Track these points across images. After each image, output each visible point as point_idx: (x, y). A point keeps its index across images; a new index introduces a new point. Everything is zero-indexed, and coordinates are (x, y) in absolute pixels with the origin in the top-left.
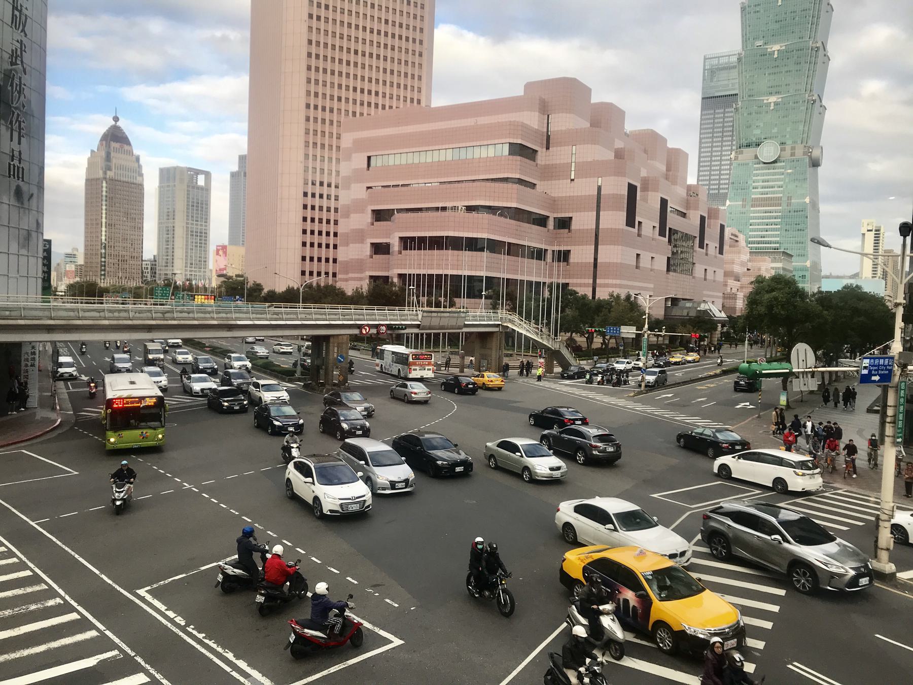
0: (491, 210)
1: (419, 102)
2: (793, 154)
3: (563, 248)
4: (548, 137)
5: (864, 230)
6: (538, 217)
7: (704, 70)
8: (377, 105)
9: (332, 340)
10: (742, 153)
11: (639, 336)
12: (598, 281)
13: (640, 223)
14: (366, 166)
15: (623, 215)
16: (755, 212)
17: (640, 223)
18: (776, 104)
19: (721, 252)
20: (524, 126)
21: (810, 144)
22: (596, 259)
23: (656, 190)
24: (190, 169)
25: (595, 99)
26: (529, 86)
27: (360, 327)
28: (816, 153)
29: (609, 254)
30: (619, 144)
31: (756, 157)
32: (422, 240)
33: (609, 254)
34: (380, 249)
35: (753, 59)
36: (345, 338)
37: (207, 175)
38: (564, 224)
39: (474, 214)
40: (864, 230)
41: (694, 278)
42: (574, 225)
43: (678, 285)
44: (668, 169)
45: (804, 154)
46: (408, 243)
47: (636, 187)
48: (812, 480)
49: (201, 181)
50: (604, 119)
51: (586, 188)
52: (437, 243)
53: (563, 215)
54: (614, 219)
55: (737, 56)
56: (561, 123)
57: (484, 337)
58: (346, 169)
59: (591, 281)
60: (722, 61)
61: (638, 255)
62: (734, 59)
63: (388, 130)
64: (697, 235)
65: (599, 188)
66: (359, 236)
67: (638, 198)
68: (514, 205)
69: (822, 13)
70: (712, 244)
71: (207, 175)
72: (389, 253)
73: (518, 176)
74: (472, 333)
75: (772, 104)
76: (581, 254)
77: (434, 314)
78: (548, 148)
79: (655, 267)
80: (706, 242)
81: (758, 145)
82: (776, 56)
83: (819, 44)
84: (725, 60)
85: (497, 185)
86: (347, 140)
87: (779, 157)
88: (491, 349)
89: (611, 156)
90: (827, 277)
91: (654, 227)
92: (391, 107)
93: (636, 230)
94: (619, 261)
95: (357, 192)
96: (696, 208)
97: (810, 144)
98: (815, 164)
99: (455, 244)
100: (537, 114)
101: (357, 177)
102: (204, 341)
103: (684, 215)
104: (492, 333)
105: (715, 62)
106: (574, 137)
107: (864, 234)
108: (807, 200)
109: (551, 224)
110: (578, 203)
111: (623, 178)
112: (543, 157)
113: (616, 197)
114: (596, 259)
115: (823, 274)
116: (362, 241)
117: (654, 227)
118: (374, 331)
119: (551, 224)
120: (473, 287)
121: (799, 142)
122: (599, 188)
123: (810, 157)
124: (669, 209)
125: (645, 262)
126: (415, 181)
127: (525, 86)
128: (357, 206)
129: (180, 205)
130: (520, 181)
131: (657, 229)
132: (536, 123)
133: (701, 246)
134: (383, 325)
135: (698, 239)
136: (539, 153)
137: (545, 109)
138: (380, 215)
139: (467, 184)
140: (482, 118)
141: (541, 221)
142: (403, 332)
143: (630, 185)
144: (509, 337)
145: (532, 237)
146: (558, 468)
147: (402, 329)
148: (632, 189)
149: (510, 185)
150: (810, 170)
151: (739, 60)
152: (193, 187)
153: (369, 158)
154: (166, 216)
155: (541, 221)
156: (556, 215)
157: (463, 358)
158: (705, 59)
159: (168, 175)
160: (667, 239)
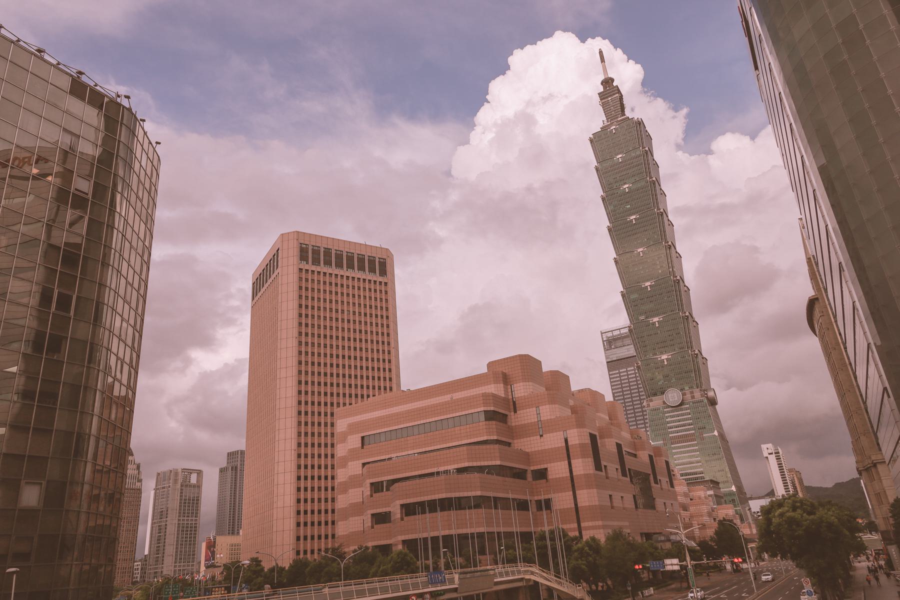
0: (480, 469)
4: (514, 403)
10: (651, 401)
12: (582, 525)
13: (605, 466)
16: (675, 448)
17: (605, 466)
20: (495, 396)
21: (704, 387)
22: (576, 505)
24: (184, 470)
26: (490, 365)
28: (711, 394)
31: (664, 403)
32: (421, 504)
34: (381, 519)
35: (638, 332)
37: (199, 473)
38: (542, 474)
42: (551, 475)
45: (702, 396)
47: (595, 436)
49: (194, 479)
51: (553, 440)
52: (433, 506)
53: (539, 467)
54: (582, 466)
56: (521, 390)
59: (576, 525)
61: (610, 496)
62: (626, 330)
63: (424, 402)
64: (649, 471)
65: (566, 441)
66: (356, 509)
68: (498, 463)
71: (199, 473)
72: (390, 521)
73: (495, 438)
76: (562, 500)
77: (468, 575)
78: (515, 412)
80: (658, 478)
81: (663, 393)
84: (617, 333)
86: (341, 425)
93: (603, 474)
95: (354, 468)
97: (704, 387)
98: (713, 402)
100: (502, 385)
101: (353, 455)
103: (635, 456)
104: (516, 589)
105: (610, 334)
106: (534, 402)
108: (716, 433)
109: (529, 476)
110: (551, 455)
111: (585, 430)
113: (582, 446)
114: (576, 505)
115: (748, 496)
119: (529, 476)
122: (566, 441)
126: (395, 455)
128: (354, 482)
129: (174, 503)
133: (656, 483)
134: (426, 593)
137: (506, 380)
138: (377, 487)
141: (520, 474)
145: (511, 490)
148: (593, 437)
149: (492, 446)
152: (186, 486)
153: (363, 438)
154: (160, 514)
155: (520, 474)
156: (532, 468)
158: (602, 333)
159: (161, 478)
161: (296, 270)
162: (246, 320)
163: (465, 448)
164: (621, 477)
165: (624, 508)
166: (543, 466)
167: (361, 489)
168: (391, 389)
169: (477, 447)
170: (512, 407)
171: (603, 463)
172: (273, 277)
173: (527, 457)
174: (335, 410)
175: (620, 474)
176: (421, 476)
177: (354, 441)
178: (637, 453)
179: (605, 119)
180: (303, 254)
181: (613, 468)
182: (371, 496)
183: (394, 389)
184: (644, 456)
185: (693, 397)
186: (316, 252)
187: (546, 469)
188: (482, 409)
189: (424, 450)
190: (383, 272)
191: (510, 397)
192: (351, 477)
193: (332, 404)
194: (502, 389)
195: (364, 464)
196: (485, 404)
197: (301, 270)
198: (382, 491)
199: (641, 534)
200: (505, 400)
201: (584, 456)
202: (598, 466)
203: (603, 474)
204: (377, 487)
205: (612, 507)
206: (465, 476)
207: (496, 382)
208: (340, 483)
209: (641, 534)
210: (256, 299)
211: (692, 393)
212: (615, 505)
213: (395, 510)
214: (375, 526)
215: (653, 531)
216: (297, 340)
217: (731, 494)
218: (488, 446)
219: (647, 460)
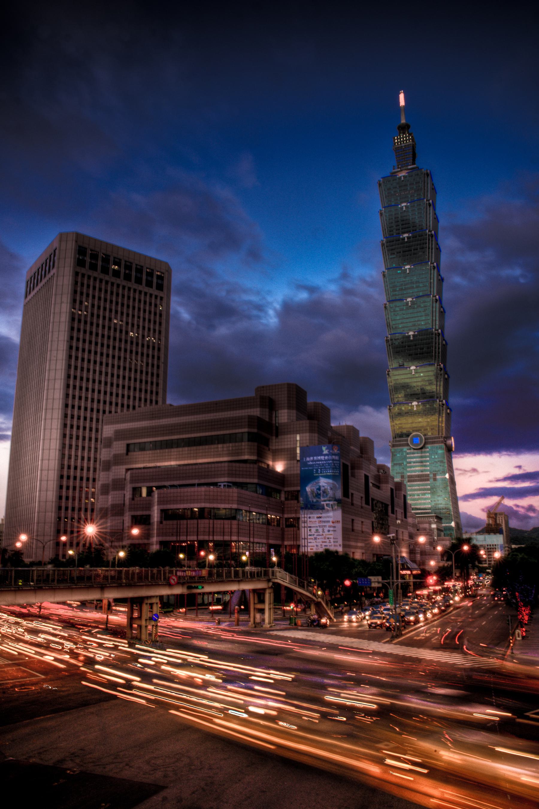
11: (353, 622)
14: (125, 452)
17: (352, 494)
18: (408, 238)
44: (362, 452)
47: (348, 466)
58: (105, 454)
61: (353, 520)
64: (389, 503)
70: (400, 511)
75: (402, 178)
86: (108, 431)
91: (362, 497)
92: (110, 412)
100: (267, 410)
102: (411, 384)
117: (362, 497)
131: (364, 499)
132: (267, 417)
133: (393, 512)
135: (390, 507)
153: (128, 445)
162: (439, 227)
164: (364, 505)
165: (362, 532)
167: (123, 492)
168: (157, 402)
169: (237, 465)
170: (274, 431)
171: (351, 491)
175: (364, 502)
176: (181, 486)
180: (81, 251)
181: (358, 496)
183: (160, 403)
184: (386, 488)
186: (94, 256)
190: (160, 287)
194: (267, 413)
195: (127, 470)
196: (250, 426)
199: (374, 555)
202: (346, 492)
203: (349, 500)
206: (486, 470)
209: (374, 555)
210: (29, 297)
212: (355, 528)
214: (164, 522)
215: (382, 553)
217: (450, 528)
218: (248, 465)
219: (389, 493)
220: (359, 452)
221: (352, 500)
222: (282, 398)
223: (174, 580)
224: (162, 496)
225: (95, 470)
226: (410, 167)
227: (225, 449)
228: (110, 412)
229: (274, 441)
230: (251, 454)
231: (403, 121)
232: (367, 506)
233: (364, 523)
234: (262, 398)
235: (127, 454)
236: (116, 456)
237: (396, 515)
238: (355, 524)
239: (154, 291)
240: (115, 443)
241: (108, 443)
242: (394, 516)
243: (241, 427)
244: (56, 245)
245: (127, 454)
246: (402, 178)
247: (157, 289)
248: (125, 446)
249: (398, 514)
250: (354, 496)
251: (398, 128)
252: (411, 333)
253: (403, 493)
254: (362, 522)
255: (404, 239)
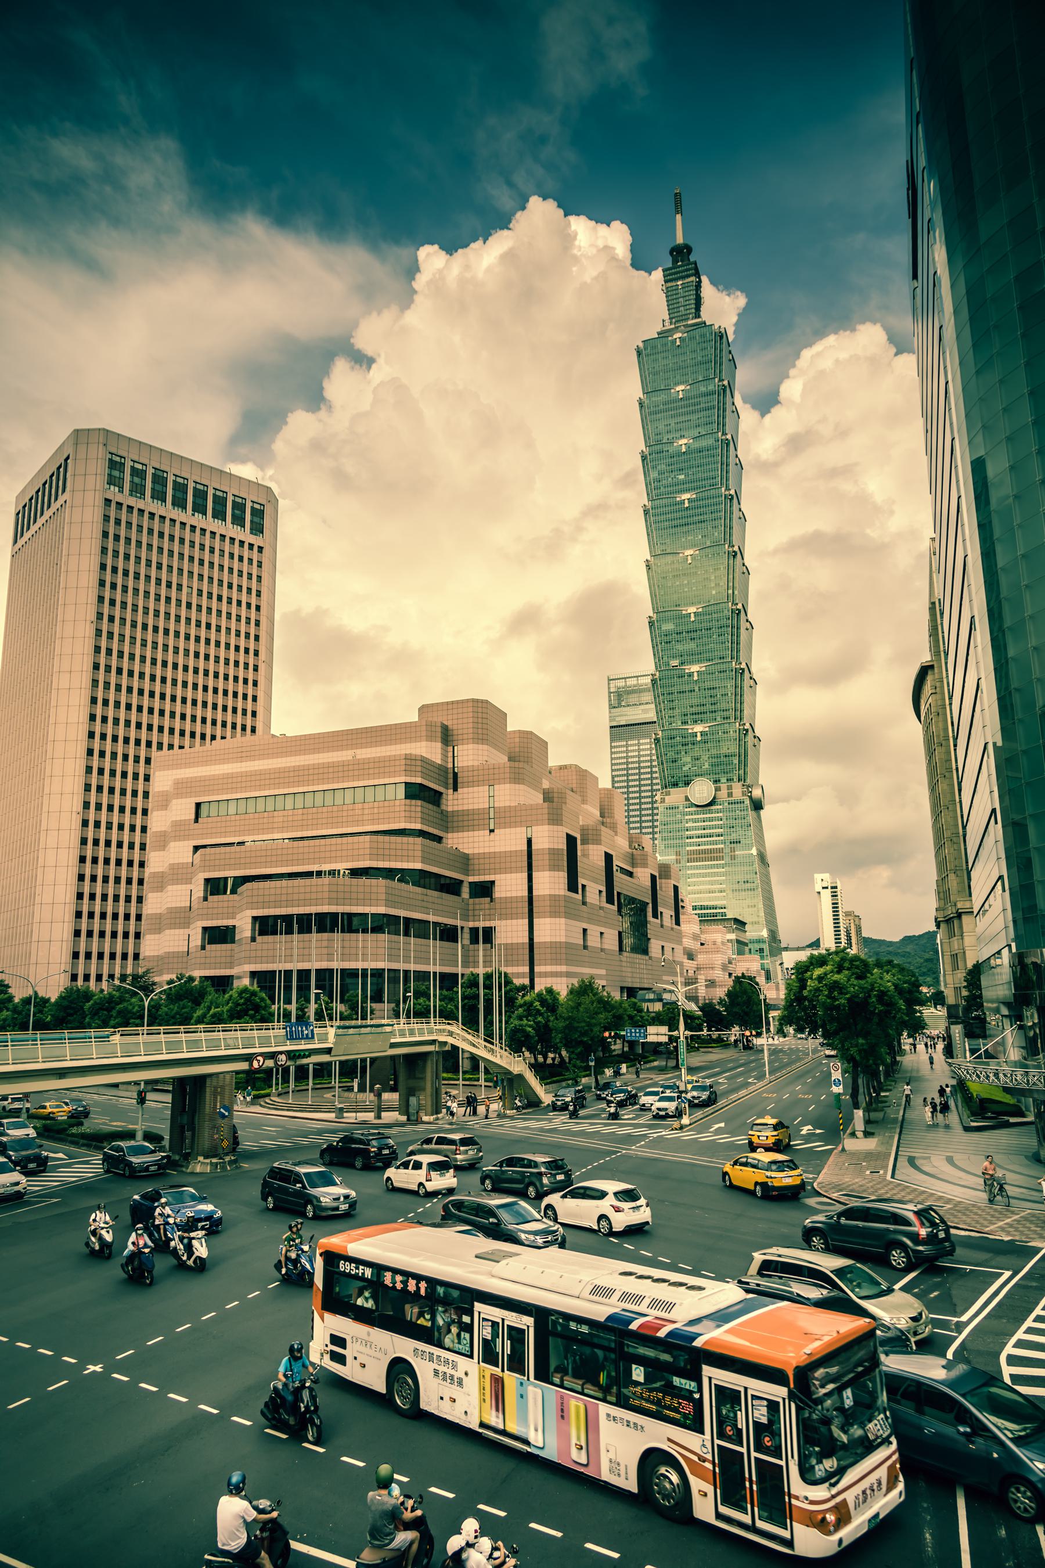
0: (389, 874)
1: (253, 730)
2: (730, 795)
3: (481, 924)
4: (455, 775)
5: (818, 888)
6: (448, 881)
7: (610, 693)
8: (193, 735)
9: (208, 1081)
12: (537, 969)
13: (584, 886)
14: (193, 816)
15: (562, 876)
17: (584, 886)
19: (678, 923)
20: (424, 760)
21: (748, 782)
23: (598, 842)
25: (513, 725)
27: (249, 1058)
28: (757, 793)
29: (550, 930)
30: (546, 784)
31: (687, 799)
32: (287, 919)
33: (550, 930)
36: (228, 1077)
38: (484, 890)
39: (363, 881)
40: (818, 888)
41: (650, 958)
42: (498, 892)
43: (634, 971)
44: (602, 815)
45: (743, 794)
46: (265, 926)
47: (575, 839)
48: (637, 1213)
50: (525, 754)
51: (510, 840)
54: (550, 883)
55: (650, 677)
56: (468, 756)
57: (414, 1062)
59: (527, 969)
60: (631, 682)
61: (585, 930)
64: (649, 901)
65: (529, 842)
66: (180, 918)
67: (579, 853)
68: (418, 866)
69: (742, 630)
72: (233, 941)
73: (418, 826)
74: (399, 1056)
75: (699, 734)
76: (510, 931)
78: (455, 789)
79: (606, 946)
82: (696, 678)
83: (743, 666)
84: (633, 681)
85: (393, 839)
86: (162, 780)
87: (714, 798)
88: (424, 1079)
89: (539, 798)
90: (786, 949)
91: (600, 892)
92: (213, 738)
93: (579, 897)
94: (563, 940)
95: (180, 852)
96: (645, 865)
99: (326, 923)
100: (439, 745)
101: (178, 831)
103: (631, 874)
104: (425, 1055)
105: (621, 683)
106: (488, 777)
107: (819, 893)
108: (754, 851)
110: (501, 862)
112: (452, 802)
113: (553, 852)
115: (783, 945)
116: (186, 924)
117: (600, 892)
118: (270, 1063)
120: (380, 985)
121: (736, 779)
122: (529, 842)
123: (751, 797)
124: (615, 868)
125: (593, 941)
127: (419, 709)
128: (178, 874)
130: (422, 833)
131: (604, 894)
132: (439, 756)
133: (655, 916)
134: (281, 1053)
136: (444, 796)
137: (447, 737)
138: (215, 886)
139: (333, 840)
140: (364, 750)
141: (452, 887)
142: (305, 1061)
143: (652, 875)
144: (450, 1057)
145: (434, 909)
146: (17, 1184)
147: (305, 1056)
148: (571, 841)
149: (411, 839)
150: (751, 814)
151: (654, 681)
153: (198, 805)
155: (452, 887)
156: (471, 879)
157: (379, 1095)
158: (609, 680)
160: (615, 908)
161: (99, 502)
163: (367, 838)
166: (491, 878)
167: (189, 887)
170: (451, 781)
171: (581, 881)
172: (55, 506)
173: (465, 861)
174: (155, 753)
175: (604, 899)
177: (183, 809)
178: (634, 870)
179: (667, 317)
181: (594, 890)
182: (205, 899)
184: (643, 875)
185: (730, 795)
187: (493, 882)
188: (403, 779)
189: (299, 834)
190: (258, 529)
191: (450, 765)
192: (172, 867)
193: (149, 744)
194: (439, 751)
195: (196, 848)
197: (108, 501)
198: (225, 893)
199: (622, 988)
200: (442, 770)
201: (554, 867)
202: (573, 885)
203: (579, 897)
204: (215, 886)
205: (585, 947)
207: (430, 738)
208: (154, 875)
209: (622, 988)
211: (730, 788)
213: (244, 926)
214: (210, 898)
216: (93, 627)
219: (648, 883)
220: (598, 813)
221: (583, 896)
222: (461, 725)
223: (259, 1061)
224: (180, 786)
225: (143, 847)
226: (690, 322)
227: (366, 812)
228: (171, 747)
229: (450, 797)
230: (409, 818)
231: (680, 240)
232: (655, 920)
233: (605, 936)
234: (430, 725)
235: (196, 820)
236: (176, 824)
237: (662, 920)
238: (589, 938)
239: (244, 534)
240: (174, 801)
241: (203, 1228)
242: (658, 921)
243: (394, 774)
244: (69, 450)
245: (196, 820)
246: (699, 734)
247: (251, 533)
248: (194, 806)
249: (664, 919)
250: (587, 888)
251: (671, 253)
252: (692, 610)
253: (673, 882)
254: (602, 933)
255: (695, 735)
